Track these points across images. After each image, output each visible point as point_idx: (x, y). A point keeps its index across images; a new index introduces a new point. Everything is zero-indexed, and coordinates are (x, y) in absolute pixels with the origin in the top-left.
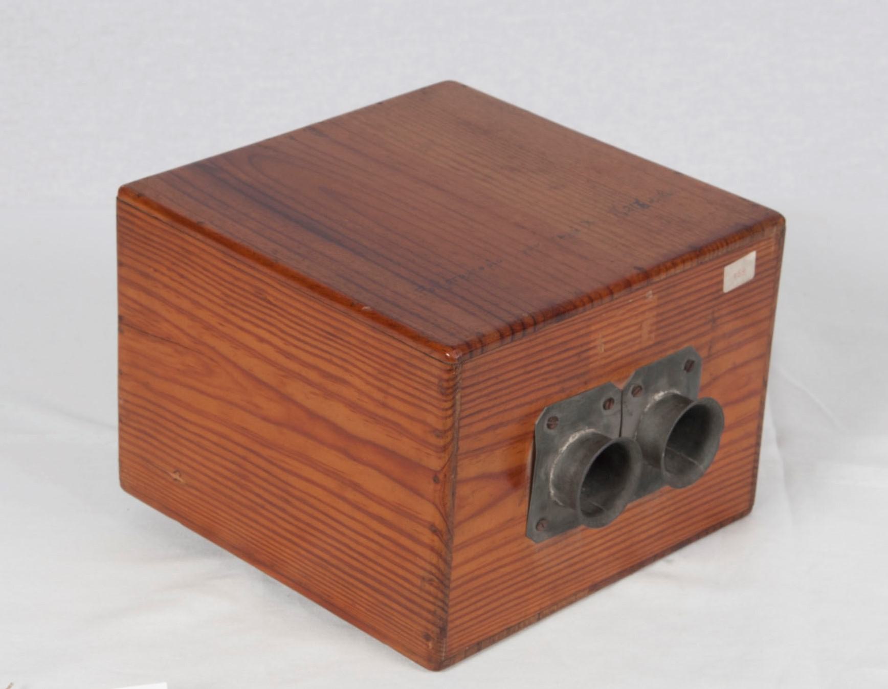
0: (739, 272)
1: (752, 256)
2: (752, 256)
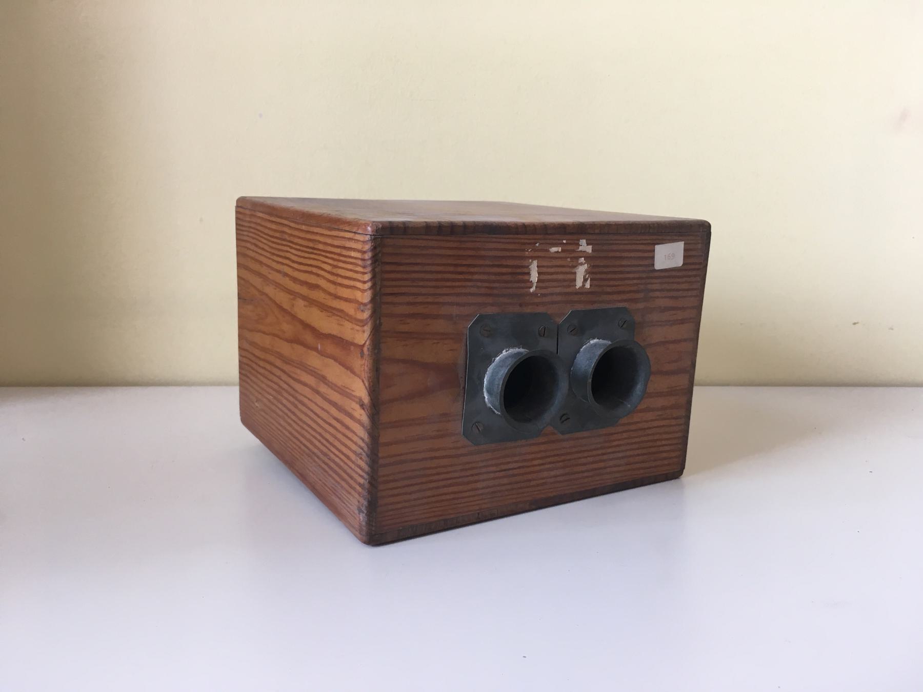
0: (668, 256)
1: (681, 245)
2: (681, 245)
